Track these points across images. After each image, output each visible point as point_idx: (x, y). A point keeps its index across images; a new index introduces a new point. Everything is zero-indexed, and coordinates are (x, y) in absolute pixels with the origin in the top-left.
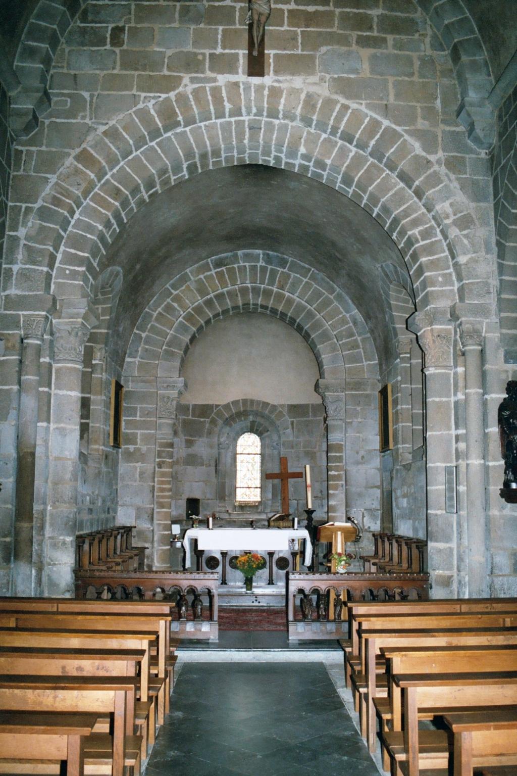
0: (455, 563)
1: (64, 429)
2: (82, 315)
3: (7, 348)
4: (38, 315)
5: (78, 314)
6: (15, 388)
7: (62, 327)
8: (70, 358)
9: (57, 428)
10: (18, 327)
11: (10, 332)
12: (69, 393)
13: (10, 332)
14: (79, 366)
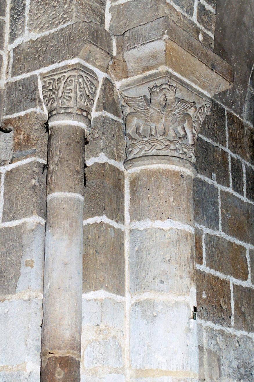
0: (64, 71)
1: (149, 303)
2: (162, 57)
3: (18, 146)
4: (66, 67)
5: (154, 56)
6: (35, 219)
7: (132, 93)
8: (154, 152)
9: (136, 304)
10: (34, 100)
11: (22, 114)
12: (158, 224)
13: (22, 114)
14: (188, 172)
